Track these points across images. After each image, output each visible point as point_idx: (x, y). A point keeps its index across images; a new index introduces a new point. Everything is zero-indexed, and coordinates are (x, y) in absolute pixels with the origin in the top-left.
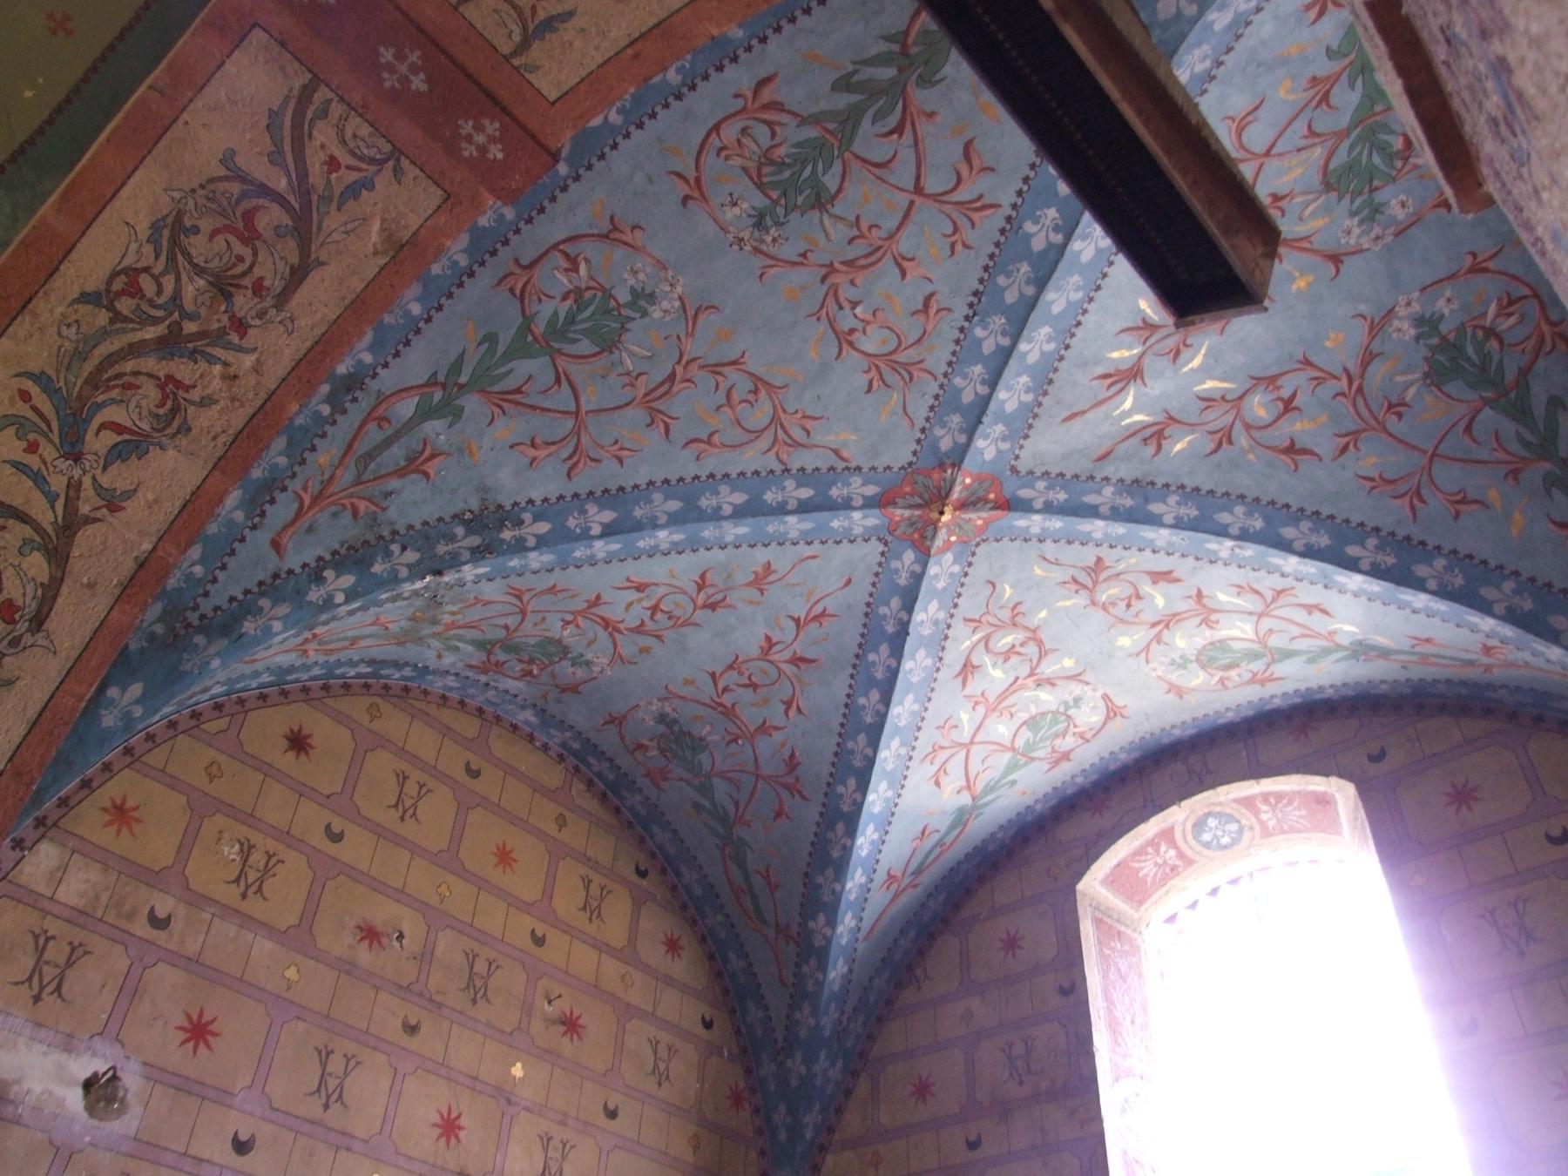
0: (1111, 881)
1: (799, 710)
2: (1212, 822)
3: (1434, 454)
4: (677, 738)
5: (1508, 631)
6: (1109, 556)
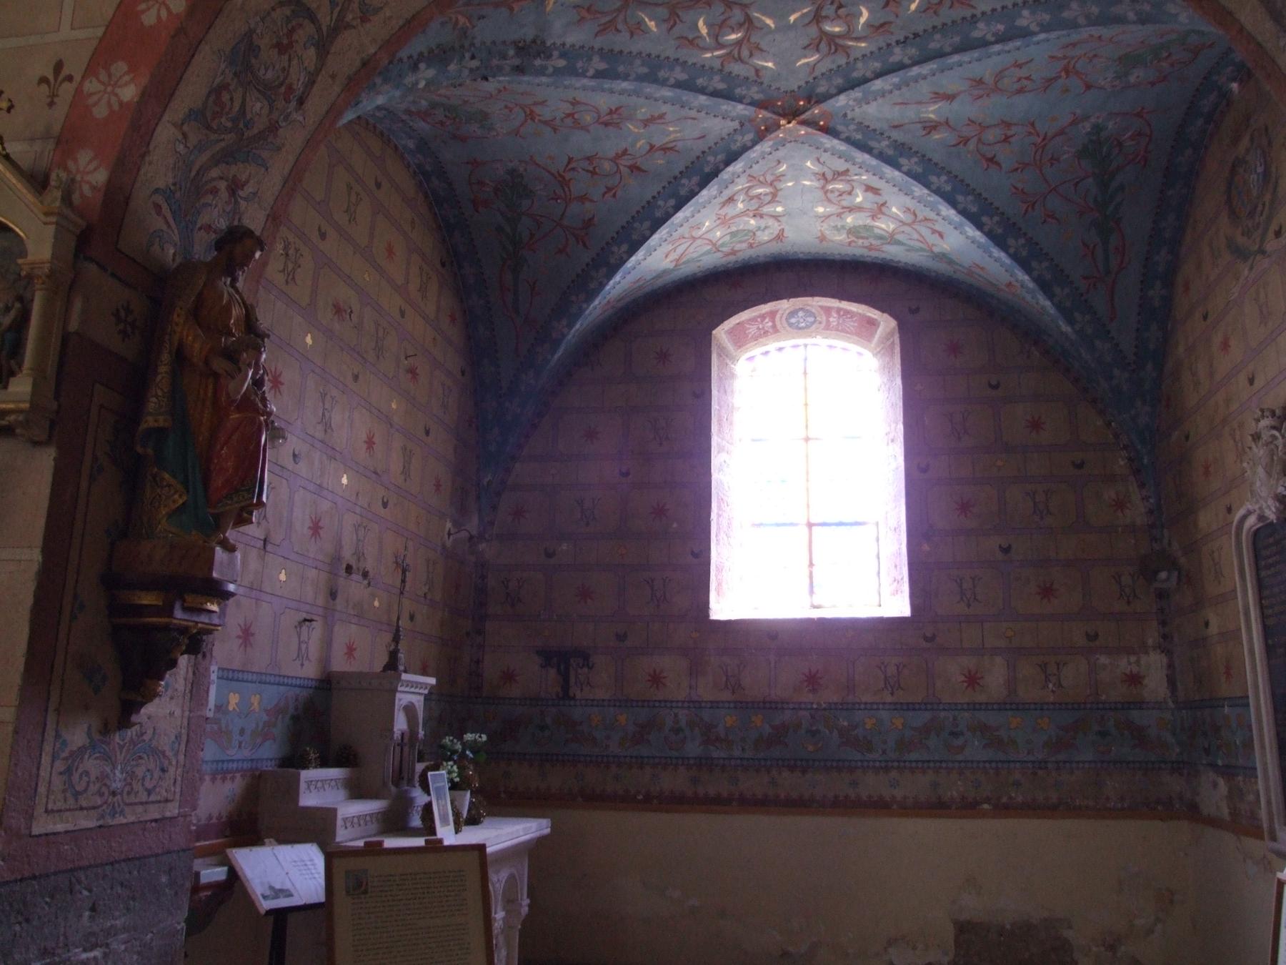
0: (731, 332)
1: (614, 195)
2: (801, 314)
3: (1054, 189)
4: (515, 186)
5: (1031, 285)
6: (854, 169)
